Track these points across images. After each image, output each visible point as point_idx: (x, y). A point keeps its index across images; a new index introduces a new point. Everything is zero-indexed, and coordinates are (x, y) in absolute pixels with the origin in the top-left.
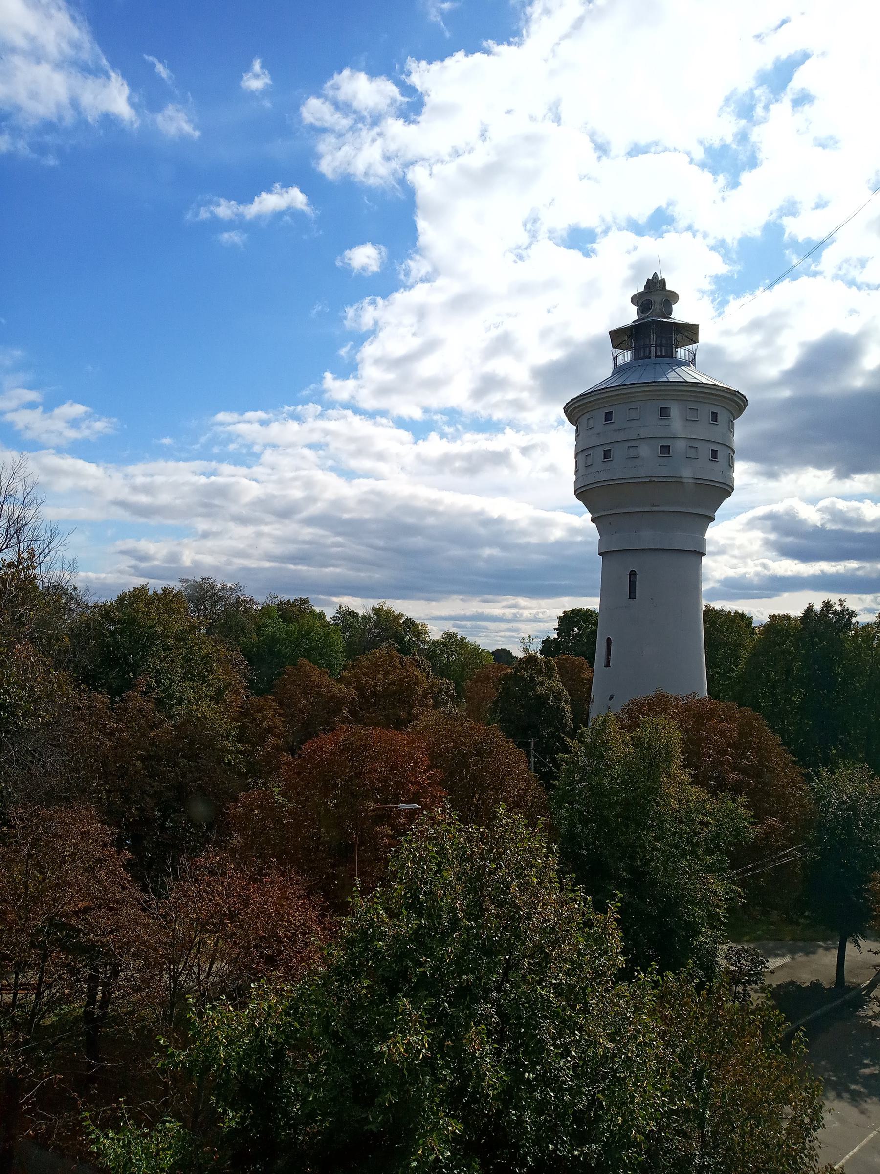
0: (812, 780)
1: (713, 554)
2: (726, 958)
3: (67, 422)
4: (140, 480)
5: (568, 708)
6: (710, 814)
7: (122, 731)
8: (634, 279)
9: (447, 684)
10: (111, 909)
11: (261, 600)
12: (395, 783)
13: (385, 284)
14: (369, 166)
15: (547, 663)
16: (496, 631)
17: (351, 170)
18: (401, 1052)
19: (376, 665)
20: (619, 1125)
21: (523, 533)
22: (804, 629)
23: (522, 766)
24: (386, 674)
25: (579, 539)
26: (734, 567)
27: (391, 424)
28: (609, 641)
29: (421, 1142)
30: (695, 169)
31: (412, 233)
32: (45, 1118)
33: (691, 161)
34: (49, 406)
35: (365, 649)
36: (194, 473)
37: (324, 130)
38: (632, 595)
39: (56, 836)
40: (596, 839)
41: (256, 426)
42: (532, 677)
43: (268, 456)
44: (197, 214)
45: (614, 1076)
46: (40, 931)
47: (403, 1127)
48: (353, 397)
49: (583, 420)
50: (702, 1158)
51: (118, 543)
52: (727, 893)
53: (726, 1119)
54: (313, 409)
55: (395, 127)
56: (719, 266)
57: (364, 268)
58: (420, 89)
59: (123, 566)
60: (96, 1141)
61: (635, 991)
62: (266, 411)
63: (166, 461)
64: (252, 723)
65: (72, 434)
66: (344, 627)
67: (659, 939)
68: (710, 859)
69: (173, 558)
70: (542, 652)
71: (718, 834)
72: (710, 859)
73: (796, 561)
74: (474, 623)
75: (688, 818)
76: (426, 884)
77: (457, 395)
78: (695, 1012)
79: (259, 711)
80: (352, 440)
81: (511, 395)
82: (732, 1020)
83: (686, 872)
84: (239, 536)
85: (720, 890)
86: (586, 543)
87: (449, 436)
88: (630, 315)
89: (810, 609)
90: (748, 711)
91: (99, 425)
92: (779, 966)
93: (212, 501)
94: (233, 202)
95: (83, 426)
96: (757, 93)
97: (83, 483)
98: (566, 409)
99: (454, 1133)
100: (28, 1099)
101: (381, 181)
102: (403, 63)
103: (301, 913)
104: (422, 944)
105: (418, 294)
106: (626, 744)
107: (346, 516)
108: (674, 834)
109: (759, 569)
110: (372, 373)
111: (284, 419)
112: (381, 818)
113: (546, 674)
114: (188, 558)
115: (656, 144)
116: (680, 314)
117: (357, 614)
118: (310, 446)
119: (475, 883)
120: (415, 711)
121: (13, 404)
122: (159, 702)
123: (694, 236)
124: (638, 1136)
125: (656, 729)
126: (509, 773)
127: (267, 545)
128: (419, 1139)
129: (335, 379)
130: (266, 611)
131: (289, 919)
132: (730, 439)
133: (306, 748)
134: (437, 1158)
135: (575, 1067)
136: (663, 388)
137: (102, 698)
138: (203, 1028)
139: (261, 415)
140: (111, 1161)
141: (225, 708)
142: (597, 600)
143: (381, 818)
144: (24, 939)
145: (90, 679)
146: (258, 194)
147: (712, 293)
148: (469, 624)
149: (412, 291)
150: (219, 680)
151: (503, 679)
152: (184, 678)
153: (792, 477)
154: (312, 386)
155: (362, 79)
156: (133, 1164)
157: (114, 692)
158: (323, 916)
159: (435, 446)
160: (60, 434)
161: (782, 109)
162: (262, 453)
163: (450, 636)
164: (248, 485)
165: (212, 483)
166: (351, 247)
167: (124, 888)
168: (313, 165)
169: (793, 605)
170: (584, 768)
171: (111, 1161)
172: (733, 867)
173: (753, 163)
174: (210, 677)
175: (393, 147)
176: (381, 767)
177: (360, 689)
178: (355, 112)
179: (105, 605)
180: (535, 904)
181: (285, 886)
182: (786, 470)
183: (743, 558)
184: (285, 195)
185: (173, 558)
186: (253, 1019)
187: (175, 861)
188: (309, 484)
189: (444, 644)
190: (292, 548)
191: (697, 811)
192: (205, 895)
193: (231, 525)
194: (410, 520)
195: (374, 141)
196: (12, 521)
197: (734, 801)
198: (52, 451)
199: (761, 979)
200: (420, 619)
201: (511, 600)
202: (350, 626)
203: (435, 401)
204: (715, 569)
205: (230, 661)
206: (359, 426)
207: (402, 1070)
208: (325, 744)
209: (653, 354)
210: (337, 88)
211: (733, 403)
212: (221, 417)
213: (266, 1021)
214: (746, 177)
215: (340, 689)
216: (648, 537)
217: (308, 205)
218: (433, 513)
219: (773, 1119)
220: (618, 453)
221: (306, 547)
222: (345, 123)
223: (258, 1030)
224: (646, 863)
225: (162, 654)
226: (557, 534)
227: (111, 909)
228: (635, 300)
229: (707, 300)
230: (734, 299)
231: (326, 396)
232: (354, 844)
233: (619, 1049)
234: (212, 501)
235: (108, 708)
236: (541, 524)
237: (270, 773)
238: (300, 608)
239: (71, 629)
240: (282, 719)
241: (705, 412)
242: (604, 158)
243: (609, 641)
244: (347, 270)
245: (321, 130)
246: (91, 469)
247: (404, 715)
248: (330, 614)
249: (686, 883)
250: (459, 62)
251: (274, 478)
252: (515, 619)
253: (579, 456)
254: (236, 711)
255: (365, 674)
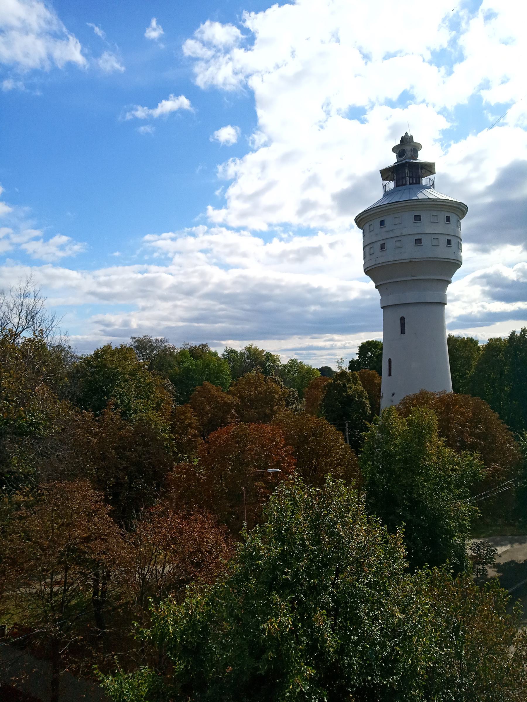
0: (519, 439)
1: (451, 301)
2: (471, 549)
3: (58, 247)
4: (102, 279)
5: (367, 402)
6: (457, 464)
7: (102, 433)
8: (392, 136)
9: (293, 391)
10: (102, 539)
11: (178, 346)
12: (265, 455)
13: (241, 150)
14: (225, 78)
15: (353, 375)
16: (321, 356)
17: (215, 82)
18: (275, 628)
19: (250, 383)
20: (409, 664)
21: (333, 295)
22: (510, 346)
23: (341, 441)
24: (256, 388)
25: (368, 297)
26: (464, 308)
27: (250, 234)
28: (390, 360)
29: (291, 681)
30: (426, 65)
31: (254, 117)
32: (74, 662)
33: (424, 61)
34: (46, 238)
35: (243, 372)
36: (134, 272)
37: (197, 59)
38: (403, 332)
39: (67, 499)
40: (387, 483)
41: (169, 242)
42: (344, 385)
43: (178, 259)
44: (124, 117)
45: (405, 635)
46: (63, 554)
47: (280, 672)
48: (225, 220)
49: (367, 227)
50: (461, 679)
51: (93, 317)
52: (470, 512)
53: (475, 655)
54: (202, 228)
55: (238, 53)
56: (445, 124)
57: (227, 141)
58: (252, 30)
59: (96, 331)
60: (102, 681)
61: (416, 581)
62: (173, 232)
63: (117, 266)
64: (178, 421)
65: (61, 254)
66: (230, 360)
67: (429, 547)
68: (458, 492)
69: (126, 323)
70: (350, 368)
71: (462, 475)
72: (458, 492)
73: (503, 303)
74: (307, 351)
75: (444, 467)
76: (285, 524)
77: (288, 215)
78: (453, 591)
79: (182, 414)
80: (226, 246)
81: (320, 212)
82: (475, 596)
83: (444, 500)
84: (163, 308)
85: (465, 510)
86: (372, 299)
87: (285, 240)
88: (392, 159)
89: (513, 333)
90: (477, 399)
91: (76, 248)
92: (504, 552)
93: (146, 288)
94: (145, 108)
95: (67, 248)
96: (461, 14)
97: (69, 283)
98: (356, 220)
99: (310, 674)
100: (64, 651)
101: (234, 88)
102: (241, 14)
103: (214, 537)
104: (284, 561)
105: (261, 155)
106: (404, 425)
107: (226, 292)
108: (435, 477)
109: (480, 309)
110: (236, 205)
111: (185, 236)
112: (258, 477)
113: (353, 382)
114: (134, 324)
115: (401, 51)
116: (423, 157)
117: (237, 352)
118: (202, 251)
119: (315, 522)
120: (274, 409)
121: (25, 239)
122: (123, 414)
123: (427, 106)
124: (422, 671)
125: (422, 415)
126: (333, 446)
127: (180, 312)
128: (290, 679)
129: (214, 210)
130: (182, 353)
131: (207, 540)
132: (458, 233)
133: (211, 437)
134: (301, 690)
135: (382, 630)
136: (415, 203)
137: (89, 415)
138: (159, 616)
139: (171, 234)
140: (112, 692)
141: (163, 414)
142: (382, 333)
143: (258, 477)
144: (53, 560)
145: (81, 403)
146: (160, 101)
147: (440, 140)
148: (304, 352)
149: (257, 153)
150: (157, 397)
151: (327, 386)
152: (137, 398)
153: (498, 251)
154: (201, 215)
155: (217, 26)
156: (125, 695)
157: (95, 409)
158: (227, 538)
159: (276, 246)
160: (54, 254)
161: (477, 22)
162: (173, 257)
163: (293, 361)
164: (166, 277)
165: (145, 278)
166: (218, 128)
167: (110, 527)
168: (192, 81)
169: (502, 331)
170: (378, 440)
171: (112, 692)
172: (472, 495)
173: (461, 58)
174: (152, 396)
175: (238, 66)
176: (257, 448)
177: (241, 398)
178: (215, 47)
179: (87, 357)
180: (352, 534)
181: (203, 522)
182: (494, 247)
183: (470, 302)
184: (177, 101)
185: (126, 323)
186: (187, 610)
187: (138, 511)
188: (203, 274)
189: (290, 366)
190: (195, 313)
191: (450, 463)
192: (156, 530)
193: (159, 302)
194: (264, 292)
195: (227, 63)
196: (28, 312)
197: (471, 455)
198: (50, 265)
199: (493, 561)
200: (274, 351)
201: (329, 336)
202: (233, 359)
203: (276, 218)
204: (453, 310)
205: (164, 385)
206: (231, 237)
207: (277, 638)
208: (222, 435)
209: (408, 182)
210: (202, 32)
211: (459, 210)
212: (148, 237)
213: (195, 610)
214: (457, 67)
215: (229, 398)
216: (411, 296)
217: (191, 106)
218: (278, 287)
219: (502, 653)
220: (389, 245)
221: (203, 312)
222: (209, 53)
223: (191, 616)
224: (420, 495)
225: (123, 384)
226: (354, 295)
227: (102, 539)
228: (394, 150)
229: (438, 145)
230: (454, 143)
231: (209, 220)
232: (242, 493)
233: (408, 618)
234: (146, 288)
235: (93, 420)
236: (344, 289)
237: (192, 451)
238: (203, 350)
239: (68, 373)
240: (196, 418)
241: (442, 216)
242: (369, 63)
243: (390, 360)
244: (217, 143)
245: (194, 60)
246: (74, 274)
247: (268, 411)
248: (220, 352)
249: (445, 507)
250: (275, 10)
251: (182, 272)
252: (332, 348)
253: (367, 248)
254: (168, 415)
255: (243, 388)
